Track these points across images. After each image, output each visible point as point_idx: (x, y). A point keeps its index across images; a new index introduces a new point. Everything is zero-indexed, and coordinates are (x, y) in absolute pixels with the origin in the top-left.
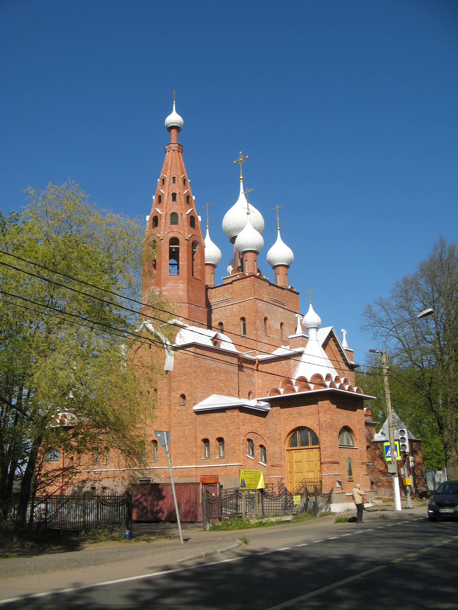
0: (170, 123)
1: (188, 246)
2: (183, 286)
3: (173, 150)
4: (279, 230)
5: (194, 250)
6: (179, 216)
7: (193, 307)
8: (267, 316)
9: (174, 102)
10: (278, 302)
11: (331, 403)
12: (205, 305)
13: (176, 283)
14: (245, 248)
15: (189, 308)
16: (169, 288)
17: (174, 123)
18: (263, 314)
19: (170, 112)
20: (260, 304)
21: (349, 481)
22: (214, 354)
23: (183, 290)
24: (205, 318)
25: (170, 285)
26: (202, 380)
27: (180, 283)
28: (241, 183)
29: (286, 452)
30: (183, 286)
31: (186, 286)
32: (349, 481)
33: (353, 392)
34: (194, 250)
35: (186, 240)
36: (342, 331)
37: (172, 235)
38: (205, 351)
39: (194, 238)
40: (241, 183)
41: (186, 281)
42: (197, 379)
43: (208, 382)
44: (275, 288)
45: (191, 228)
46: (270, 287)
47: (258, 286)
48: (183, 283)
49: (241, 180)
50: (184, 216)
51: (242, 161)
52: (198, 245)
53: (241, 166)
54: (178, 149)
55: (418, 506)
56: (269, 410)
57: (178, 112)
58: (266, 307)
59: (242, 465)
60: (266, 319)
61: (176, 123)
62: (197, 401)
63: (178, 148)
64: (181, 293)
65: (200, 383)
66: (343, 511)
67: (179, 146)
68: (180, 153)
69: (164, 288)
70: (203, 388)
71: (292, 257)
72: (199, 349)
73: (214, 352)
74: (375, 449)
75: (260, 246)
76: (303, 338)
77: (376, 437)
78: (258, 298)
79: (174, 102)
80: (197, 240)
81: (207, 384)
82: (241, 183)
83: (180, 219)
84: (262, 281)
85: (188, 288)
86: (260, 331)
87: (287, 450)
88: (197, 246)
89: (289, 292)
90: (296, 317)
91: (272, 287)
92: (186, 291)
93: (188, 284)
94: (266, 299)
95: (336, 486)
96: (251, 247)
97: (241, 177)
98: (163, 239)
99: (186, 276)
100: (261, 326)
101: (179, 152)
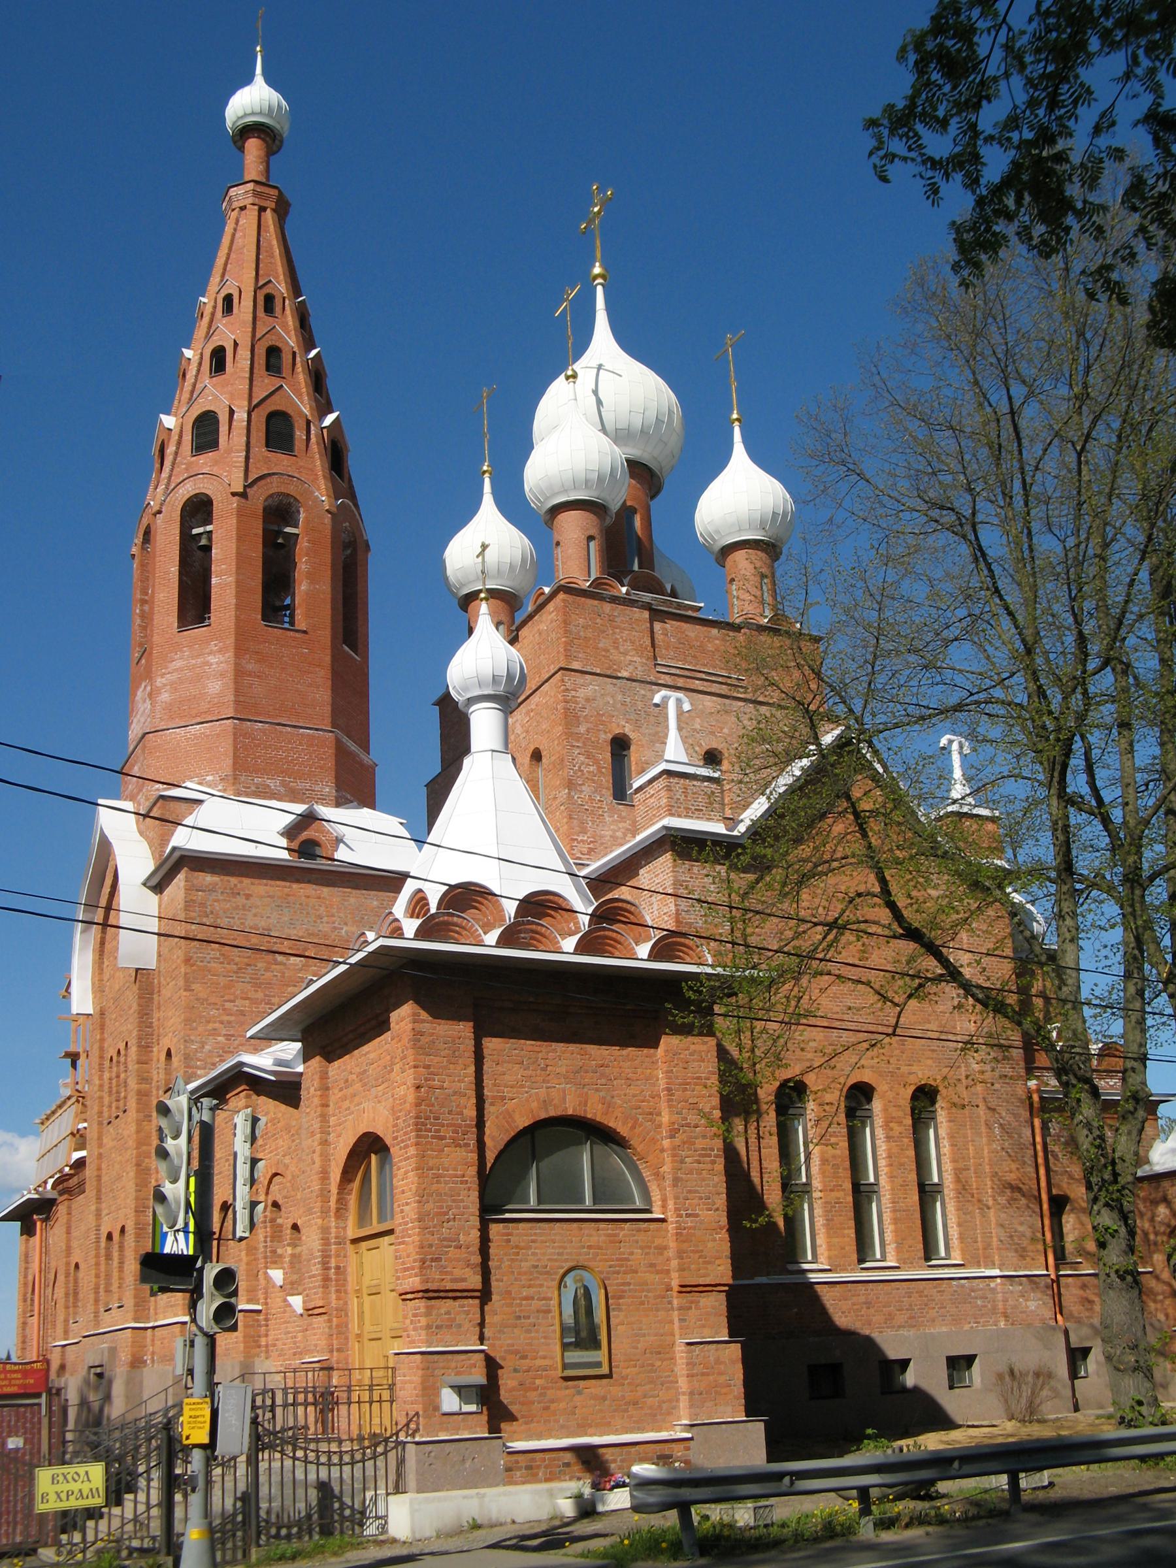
0: (241, 114)
1: (240, 513)
2: (222, 659)
3: (243, 208)
4: (737, 423)
5: (288, 530)
6: (223, 418)
7: (263, 731)
8: (628, 730)
9: (258, 48)
10: (704, 676)
11: (424, 1015)
12: (328, 720)
13: (198, 656)
14: (547, 498)
15: (237, 734)
16: (175, 676)
17: (246, 115)
18: (603, 723)
19: (248, 80)
20: (589, 688)
21: (566, 1379)
22: (295, 886)
23: (222, 675)
24: (321, 768)
25: (178, 664)
26: (228, 987)
27: (210, 654)
28: (600, 291)
29: (350, 1248)
30: (222, 659)
31: (232, 660)
32: (566, 1379)
33: (401, 936)
34: (288, 530)
35: (234, 494)
36: (944, 741)
37: (187, 491)
38: (247, 881)
39: (274, 486)
40: (600, 289)
41: (231, 641)
42: (194, 986)
43: (260, 995)
44: (685, 626)
45: (270, 455)
46: (658, 626)
47: (585, 627)
48: (220, 651)
49: (600, 281)
50: (241, 415)
51: (599, 212)
52: (302, 510)
53: (597, 233)
54: (257, 201)
55: (488, 1547)
56: (301, 1074)
57: (270, 81)
58: (620, 697)
59: (259, 1311)
60: (620, 745)
61: (253, 114)
62: (198, 1068)
63: (256, 194)
64: (215, 687)
65: (212, 1000)
66: (429, 1532)
67: (259, 189)
68: (268, 210)
69: (159, 681)
70: (232, 1018)
71: (785, 500)
72: (213, 872)
73: (298, 881)
74: (1155, 1203)
75: (600, 479)
76: (674, 780)
77: (1162, 1155)
78: (588, 669)
79: (258, 48)
80: (291, 490)
81: (254, 1002)
82: (600, 289)
83: (223, 428)
84: (607, 607)
85: (236, 664)
86: (584, 788)
87: (355, 1241)
88: (299, 512)
89: (764, 638)
90: (657, 705)
91: (671, 625)
92: (230, 675)
93: (240, 650)
94: (631, 668)
95: (437, 1408)
96: (565, 491)
97: (597, 270)
98: (160, 512)
99: (232, 625)
100: (592, 768)
101: (262, 209)
